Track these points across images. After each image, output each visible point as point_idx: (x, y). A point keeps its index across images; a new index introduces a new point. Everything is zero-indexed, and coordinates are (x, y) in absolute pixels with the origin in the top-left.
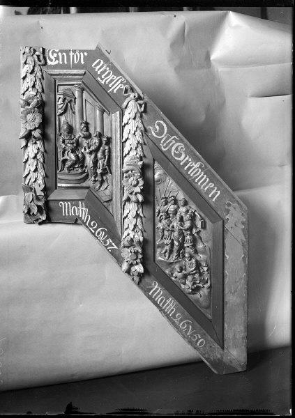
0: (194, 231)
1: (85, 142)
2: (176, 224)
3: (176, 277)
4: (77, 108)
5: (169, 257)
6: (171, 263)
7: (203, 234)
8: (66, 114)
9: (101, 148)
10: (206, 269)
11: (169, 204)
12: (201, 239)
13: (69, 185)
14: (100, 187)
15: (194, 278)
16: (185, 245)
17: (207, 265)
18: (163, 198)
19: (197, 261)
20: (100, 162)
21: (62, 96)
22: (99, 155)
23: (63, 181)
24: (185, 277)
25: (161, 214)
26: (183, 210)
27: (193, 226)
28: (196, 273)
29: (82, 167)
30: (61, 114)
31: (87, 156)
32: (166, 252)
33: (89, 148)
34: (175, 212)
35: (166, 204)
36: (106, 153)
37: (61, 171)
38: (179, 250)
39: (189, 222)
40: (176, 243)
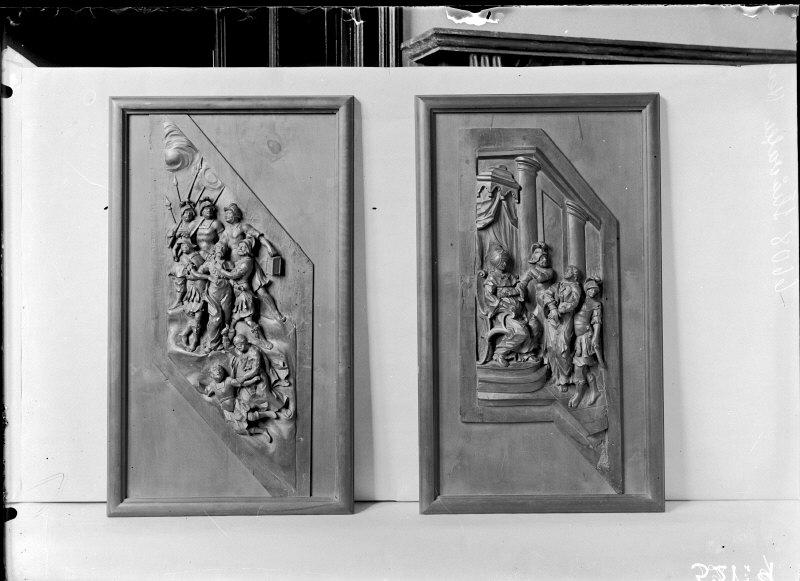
0: (257, 281)
1: (543, 295)
2: (214, 265)
3: (212, 394)
4: (521, 211)
5: (198, 344)
6: (201, 360)
7: (279, 290)
8: (495, 227)
9: (584, 307)
10: (283, 374)
11: (199, 219)
12: (274, 301)
13: (507, 396)
14: (579, 400)
15: (254, 396)
16: (236, 317)
17: (287, 364)
18: (184, 204)
19: (261, 355)
20: (582, 340)
21: (488, 184)
22: (579, 323)
23: (491, 386)
24: (235, 391)
25: (179, 241)
26: (231, 232)
27: (254, 267)
28: (257, 382)
29: (536, 352)
30: (486, 227)
31: (549, 325)
32: (190, 332)
33: (557, 305)
34: (214, 238)
35: (192, 218)
36: (596, 319)
37: (485, 362)
38: (221, 326)
39: (246, 259)
40: (212, 310)
